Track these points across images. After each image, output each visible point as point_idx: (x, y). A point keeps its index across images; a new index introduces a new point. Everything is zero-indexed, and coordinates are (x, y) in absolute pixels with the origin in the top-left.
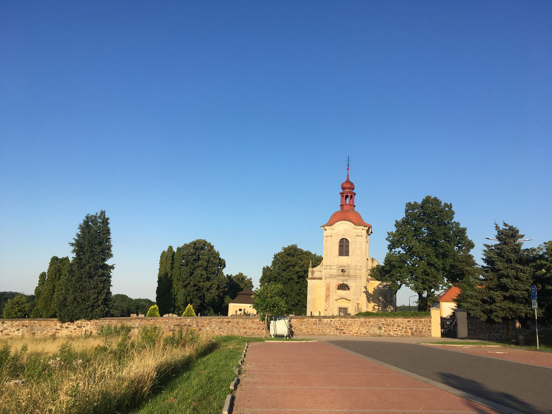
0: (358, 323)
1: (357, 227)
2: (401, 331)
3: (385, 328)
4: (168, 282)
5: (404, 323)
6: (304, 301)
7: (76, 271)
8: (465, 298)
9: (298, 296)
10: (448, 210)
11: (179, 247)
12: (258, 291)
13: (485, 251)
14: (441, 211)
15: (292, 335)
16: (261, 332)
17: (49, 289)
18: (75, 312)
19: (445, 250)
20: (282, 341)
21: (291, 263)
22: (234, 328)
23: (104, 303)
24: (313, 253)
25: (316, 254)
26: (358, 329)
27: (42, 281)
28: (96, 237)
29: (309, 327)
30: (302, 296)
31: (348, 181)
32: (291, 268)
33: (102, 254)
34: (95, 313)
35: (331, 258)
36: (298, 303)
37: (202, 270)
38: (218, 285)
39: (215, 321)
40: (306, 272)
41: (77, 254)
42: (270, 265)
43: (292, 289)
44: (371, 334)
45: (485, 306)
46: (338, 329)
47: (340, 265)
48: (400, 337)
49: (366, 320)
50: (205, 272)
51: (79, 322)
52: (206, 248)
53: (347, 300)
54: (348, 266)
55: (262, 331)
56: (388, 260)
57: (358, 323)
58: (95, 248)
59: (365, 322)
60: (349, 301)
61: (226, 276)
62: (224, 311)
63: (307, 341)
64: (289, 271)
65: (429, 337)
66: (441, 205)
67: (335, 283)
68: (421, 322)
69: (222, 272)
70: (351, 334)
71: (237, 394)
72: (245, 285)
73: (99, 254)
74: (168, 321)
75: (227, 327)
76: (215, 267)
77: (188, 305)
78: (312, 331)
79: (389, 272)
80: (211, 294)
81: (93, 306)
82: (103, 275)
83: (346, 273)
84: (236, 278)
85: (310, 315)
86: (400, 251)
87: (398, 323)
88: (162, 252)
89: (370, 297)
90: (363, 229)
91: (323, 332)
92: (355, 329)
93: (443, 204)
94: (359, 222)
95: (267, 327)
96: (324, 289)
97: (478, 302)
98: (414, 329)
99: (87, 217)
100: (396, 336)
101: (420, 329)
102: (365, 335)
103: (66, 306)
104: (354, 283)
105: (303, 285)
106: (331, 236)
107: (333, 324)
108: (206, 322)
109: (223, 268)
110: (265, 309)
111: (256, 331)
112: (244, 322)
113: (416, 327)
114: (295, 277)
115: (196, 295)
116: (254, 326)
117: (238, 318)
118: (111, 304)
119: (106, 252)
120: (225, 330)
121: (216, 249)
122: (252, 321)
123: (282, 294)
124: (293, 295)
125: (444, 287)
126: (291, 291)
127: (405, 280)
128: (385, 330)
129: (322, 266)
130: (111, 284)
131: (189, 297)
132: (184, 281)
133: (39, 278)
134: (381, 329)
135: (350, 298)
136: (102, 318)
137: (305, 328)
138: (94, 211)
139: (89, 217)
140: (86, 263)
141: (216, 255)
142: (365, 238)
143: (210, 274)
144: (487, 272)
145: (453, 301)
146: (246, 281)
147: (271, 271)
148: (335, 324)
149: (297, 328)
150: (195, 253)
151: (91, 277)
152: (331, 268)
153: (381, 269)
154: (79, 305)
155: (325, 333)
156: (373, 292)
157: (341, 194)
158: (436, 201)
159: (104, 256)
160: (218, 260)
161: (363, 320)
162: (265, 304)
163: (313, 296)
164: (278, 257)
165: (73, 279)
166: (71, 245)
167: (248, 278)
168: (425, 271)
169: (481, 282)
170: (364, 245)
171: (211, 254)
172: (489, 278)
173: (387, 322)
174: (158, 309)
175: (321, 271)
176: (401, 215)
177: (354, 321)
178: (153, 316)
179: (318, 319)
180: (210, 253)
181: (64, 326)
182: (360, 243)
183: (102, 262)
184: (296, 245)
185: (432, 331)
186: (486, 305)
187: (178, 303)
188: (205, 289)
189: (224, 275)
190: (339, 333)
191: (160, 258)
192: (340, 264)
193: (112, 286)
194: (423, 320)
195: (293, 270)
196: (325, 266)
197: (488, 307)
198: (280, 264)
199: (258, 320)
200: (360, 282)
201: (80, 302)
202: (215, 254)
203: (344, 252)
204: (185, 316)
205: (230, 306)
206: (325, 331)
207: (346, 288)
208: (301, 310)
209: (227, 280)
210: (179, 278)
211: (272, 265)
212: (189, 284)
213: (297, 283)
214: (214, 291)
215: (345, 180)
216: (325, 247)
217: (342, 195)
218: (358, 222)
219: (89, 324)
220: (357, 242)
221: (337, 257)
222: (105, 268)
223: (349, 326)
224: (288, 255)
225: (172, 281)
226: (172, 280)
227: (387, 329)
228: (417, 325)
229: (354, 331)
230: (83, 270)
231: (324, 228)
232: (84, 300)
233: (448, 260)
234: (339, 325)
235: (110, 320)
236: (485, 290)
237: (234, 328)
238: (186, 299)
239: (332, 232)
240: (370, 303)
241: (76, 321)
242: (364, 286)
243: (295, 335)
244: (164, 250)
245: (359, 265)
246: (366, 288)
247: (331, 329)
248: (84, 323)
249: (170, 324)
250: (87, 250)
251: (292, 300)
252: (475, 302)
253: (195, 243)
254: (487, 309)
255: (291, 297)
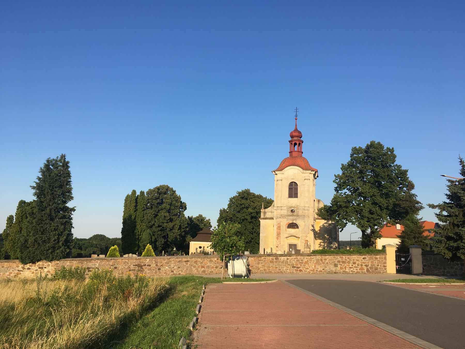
0: (314, 261)
1: (305, 171)
2: (357, 268)
3: (341, 265)
4: (132, 224)
5: (360, 260)
6: (256, 239)
7: (37, 213)
8: (409, 234)
9: (251, 235)
10: (390, 154)
11: (142, 191)
12: (215, 231)
13: (448, 186)
14: (385, 155)
15: (250, 273)
16: (219, 271)
17: (16, 231)
18: (35, 254)
19: (389, 190)
20: (241, 282)
21: (245, 206)
22: (192, 268)
23: (65, 244)
24: (264, 196)
25: (266, 197)
26: (314, 267)
27: (9, 224)
28: (56, 180)
29: (266, 265)
30: (255, 234)
31: (296, 130)
32: (245, 209)
33: (63, 196)
34: (56, 254)
35: (281, 200)
36: (251, 240)
37: (165, 212)
38: (180, 226)
39: (174, 260)
40: (259, 213)
41: (38, 197)
42: (226, 207)
43: (245, 228)
44: (327, 271)
45: (450, 243)
46: (295, 267)
47: (289, 206)
48: (356, 274)
49: (322, 257)
50: (168, 214)
51: (40, 263)
52: (169, 192)
53: (297, 237)
54: (297, 207)
55: (220, 270)
56: (335, 201)
57: (314, 261)
58: (55, 191)
59: (321, 260)
60: (298, 239)
61: (187, 218)
62: (185, 249)
63: (267, 282)
64: (243, 212)
65: (384, 273)
66: (384, 149)
67: (285, 222)
68: (377, 258)
69: (184, 214)
70: (307, 272)
71: (200, 316)
72: (205, 225)
73: (60, 197)
74: (127, 261)
75: (185, 266)
76: (177, 209)
77: (148, 245)
78: (269, 269)
79: (336, 211)
80: (174, 233)
81: (54, 248)
82: (64, 217)
83: (295, 214)
84: (196, 219)
85: (263, 254)
86: (346, 192)
87: (354, 260)
88: (126, 195)
89: (317, 235)
90: (310, 173)
91: (280, 270)
92: (311, 266)
93: (385, 148)
94: (306, 166)
95: (225, 266)
96: (276, 227)
97: (443, 239)
98: (370, 266)
99: (48, 161)
100: (351, 273)
101: (375, 266)
102: (321, 272)
103: (28, 248)
104: (303, 222)
105: (256, 224)
106: (281, 180)
107: (290, 262)
108: (165, 261)
109: (185, 210)
110: (223, 249)
111: (214, 270)
112: (202, 261)
113: (372, 264)
114: (248, 218)
115: (161, 235)
116: (212, 265)
117: (196, 257)
118: (73, 245)
119: (67, 195)
120: (184, 269)
121: (178, 193)
122: (210, 260)
123: (238, 233)
124: (247, 234)
125: (388, 224)
126: (245, 230)
127: (352, 219)
128: (340, 267)
129: (273, 207)
130: (73, 225)
131: (154, 236)
132: (149, 222)
133: (7, 221)
134: (337, 266)
135: (299, 235)
136: (63, 259)
137: (262, 267)
138: (55, 155)
139: (50, 161)
140: (46, 205)
141: (178, 199)
142: (312, 181)
143: (173, 216)
144: (451, 207)
145: (397, 237)
146: (205, 221)
147: (227, 213)
148: (292, 262)
149: (254, 266)
150: (159, 197)
151: (52, 219)
152: (281, 209)
153: (328, 209)
154: (40, 247)
155: (282, 271)
156: (319, 230)
157: (290, 142)
158: (380, 146)
159: (65, 198)
160: (179, 203)
161: (319, 257)
162: (223, 244)
163: (265, 234)
164: (233, 200)
165: (34, 221)
166: (32, 189)
167: (207, 219)
168: (370, 210)
169: (446, 219)
170: (312, 188)
171: (174, 198)
172: (454, 214)
173: (343, 259)
174: (118, 249)
175: (272, 212)
176: (346, 160)
177: (311, 258)
178: (113, 257)
179: (275, 257)
180: (172, 197)
181: (26, 268)
182: (307, 185)
183: (62, 204)
184: (249, 190)
185: (387, 268)
186: (451, 242)
187: (144, 242)
188: (168, 229)
189: (185, 216)
190: (296, 271)
191: (124, 201)
192: (290, 205)
193: (74, 228)
194: (378, 257)
195: (247, 211)
196: (276, 207)
197: (452, 244)
198: (235, 206)
199: (216, 259)
200: (308, 221)
201: (41, 243)
202: (177, 198)
203: (293, 193)
204: (144, 256)
205: (191, 244)
206: (282, 269)
207: (295, 227)
208: (254, 247)
209: (188, 221)
210: (142, 220)
211: (228, 207)
212: (154, 225)
213: (250, 222)
214: (176, 231)
215: (294, 129)
216: (276, 190)
217: (291, 142)
218: (306, 167)
219: (51, 265)
220: (305, 185)
221: (287, 199)
222: (66, 210)
223: (305, 264)
224: (242, 198)
225: (135, 222)
226: (136, 221)
227: (343, 266)
228: (372, 262)
229: (310, 269)
230: (44, 212)
231: (275, 172)
232: (44, 241)
233: (391, 200)
234: (295, 263)
235: (71, 261)
236: (450, 226)
237: (192, 268)
238: (151, 238)
239: (283, 176)
240: (316, 240)
241: (38, 262)
242: (312, 225)
243: (252, 273)
244: (128, 194)
245: (307, 205)
246: (313, 226)
247: (288, 267)
248: (45, 264)
249: (129, 265)
250: (48, 193)
251: (246, 238)
252: (438, 239)
253: (158, 188)
254: (453, 247)
255: (245, 235)
